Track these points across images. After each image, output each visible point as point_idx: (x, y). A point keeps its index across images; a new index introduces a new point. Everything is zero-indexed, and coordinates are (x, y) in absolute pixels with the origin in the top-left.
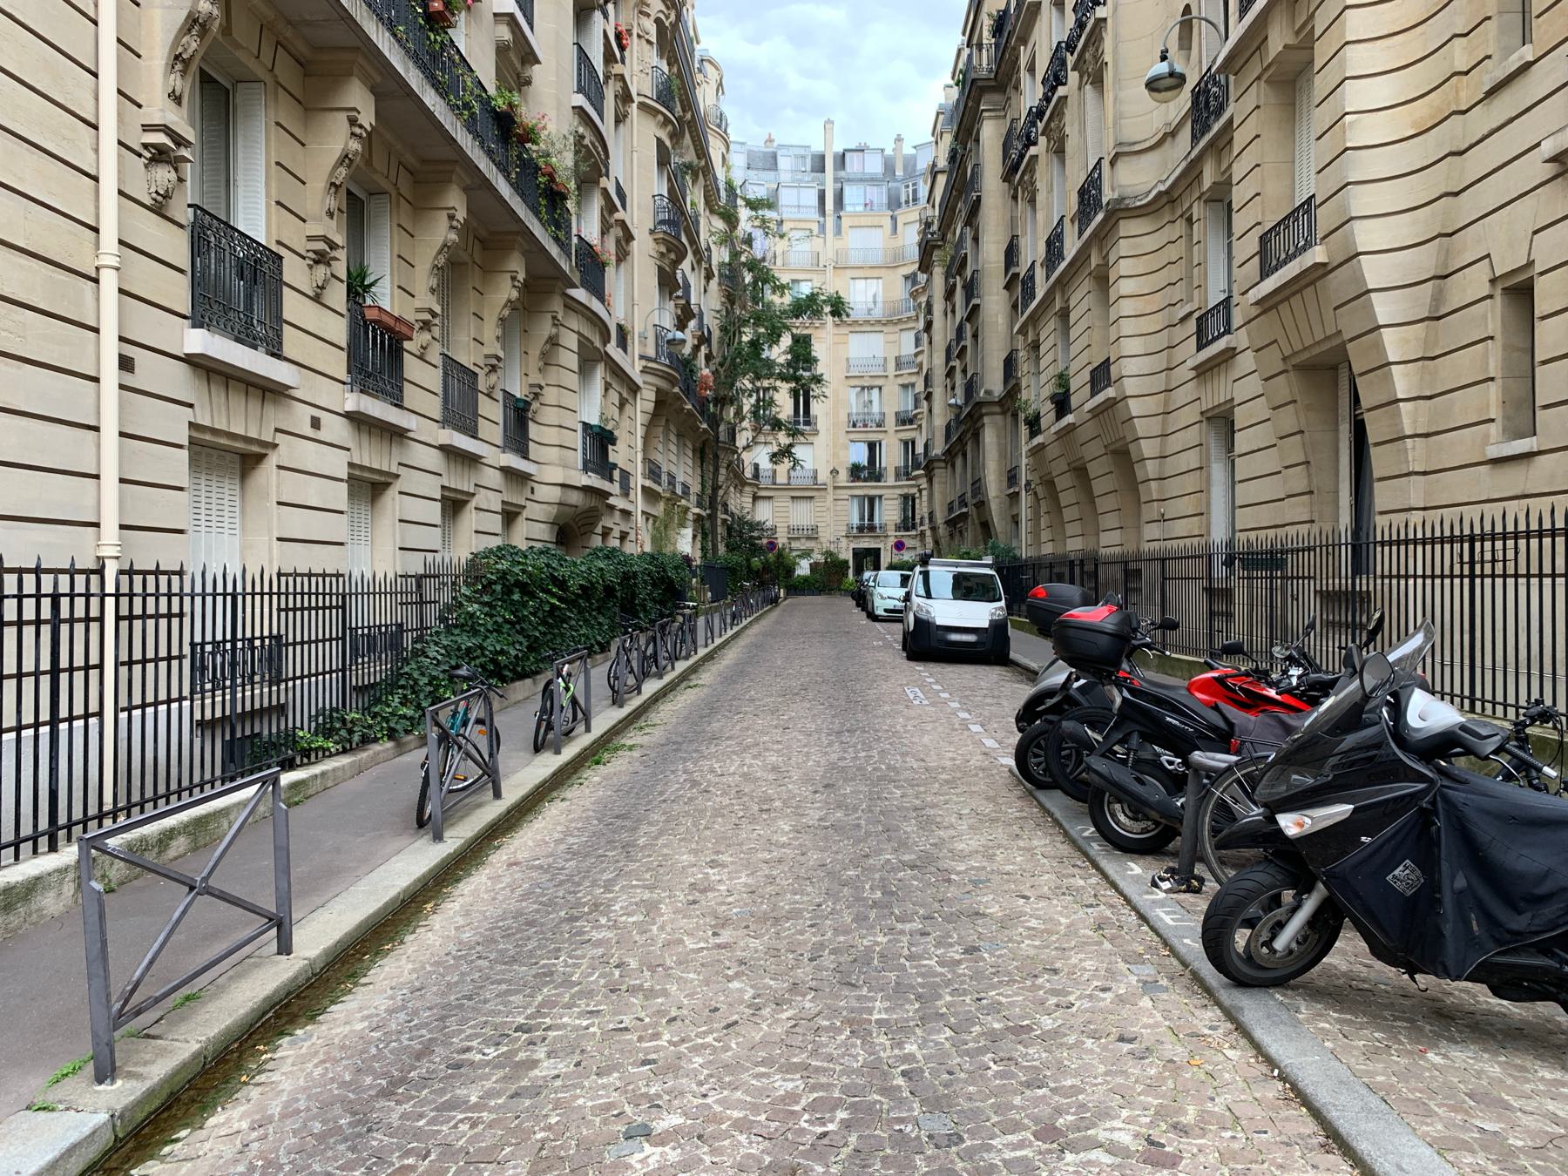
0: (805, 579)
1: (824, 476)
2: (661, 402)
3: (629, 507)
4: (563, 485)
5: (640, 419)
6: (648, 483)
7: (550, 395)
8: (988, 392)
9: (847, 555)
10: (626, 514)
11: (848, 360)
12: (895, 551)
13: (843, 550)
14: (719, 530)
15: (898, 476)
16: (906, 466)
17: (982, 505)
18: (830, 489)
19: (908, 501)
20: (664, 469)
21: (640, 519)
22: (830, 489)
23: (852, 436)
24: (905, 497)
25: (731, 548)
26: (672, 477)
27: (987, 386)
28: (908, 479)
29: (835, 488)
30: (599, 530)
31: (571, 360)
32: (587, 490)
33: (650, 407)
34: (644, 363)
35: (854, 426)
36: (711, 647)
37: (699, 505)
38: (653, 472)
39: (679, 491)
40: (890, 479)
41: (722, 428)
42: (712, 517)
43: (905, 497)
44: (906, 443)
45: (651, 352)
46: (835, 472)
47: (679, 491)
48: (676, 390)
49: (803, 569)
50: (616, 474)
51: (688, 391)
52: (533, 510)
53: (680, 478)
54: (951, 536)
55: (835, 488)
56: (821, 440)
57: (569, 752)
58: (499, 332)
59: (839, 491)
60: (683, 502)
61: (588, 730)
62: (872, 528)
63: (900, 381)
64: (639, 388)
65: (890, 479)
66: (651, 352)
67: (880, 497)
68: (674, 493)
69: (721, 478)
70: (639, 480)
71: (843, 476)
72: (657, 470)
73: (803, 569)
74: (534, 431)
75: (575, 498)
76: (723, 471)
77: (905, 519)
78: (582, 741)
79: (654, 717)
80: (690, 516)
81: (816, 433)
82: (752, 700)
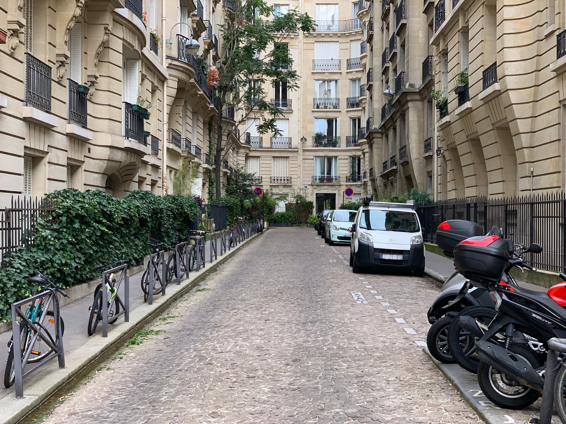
0: (282, 215)
1: (296, 142)
2: (181, 89)
3: (158, 163)
4: (111, 147)
5: (167, 101)
6: (172, 146)
7: (103, 83)
8: (411, 85)
9: (312, 198)
10: (156, 168)
11: (313, 61)
12: (346, 196)
13: (309, 195)
14: (222, 180)
15: (348, 143)
16: (354, 136)
17: (406, 164)
18: (300, 152)
19: (356, 161)
20: (183, 136)
21: (166, 172)
22: (300, 152)
23: (316, 115)
24: (353, 158)
25: (229, 192)
26: (188, 142)
27: (411, 81)
28: (355, 146)
29: (304, 151)
30: (136, 179)
31: (118, 59)
32: (127, 150)
33: (174, 92)
34: (169, 61)
35: (318, 107)
36: (215, 263)
37: (207, 162)
38: (175, 138)
39: (193, 151)
40: (343, 145)
41: (224, 108)
42: (217, 170)
43: (353, 158)
44: (354, 120)
45: (175, 54)
46: (304, 139)
47: (193, 151)
48: (192, 80)
49: (281, 208)
50: (149, 139)
51: (200, 81)
52: (89, 164)
53: (194, 143)
54: (385, 185)
55: (304, 151)
56: (294, 117)
57: (113, 335)
58: (67, 38)
59: (307, 153)
60: (196, 160)
61: (127, 320)
62: (330, 179)
63: (351, 76)
64: (165, 79)
65: (343, 145)
66: (175, 54)
67: (336, 157)
68: (189, 153)
69: (223, 143)
70: (165, 144)
71: (310, 142)
72: (178, 137)
73: (281, 208)
74: (91, 108)
75: (120, 156)
76: (224, 138)
77: (353, 173)
78: (122, 328)
79: (173, 311)
80: (201, 170)
81: (291, 112)
82: (243, 300)
